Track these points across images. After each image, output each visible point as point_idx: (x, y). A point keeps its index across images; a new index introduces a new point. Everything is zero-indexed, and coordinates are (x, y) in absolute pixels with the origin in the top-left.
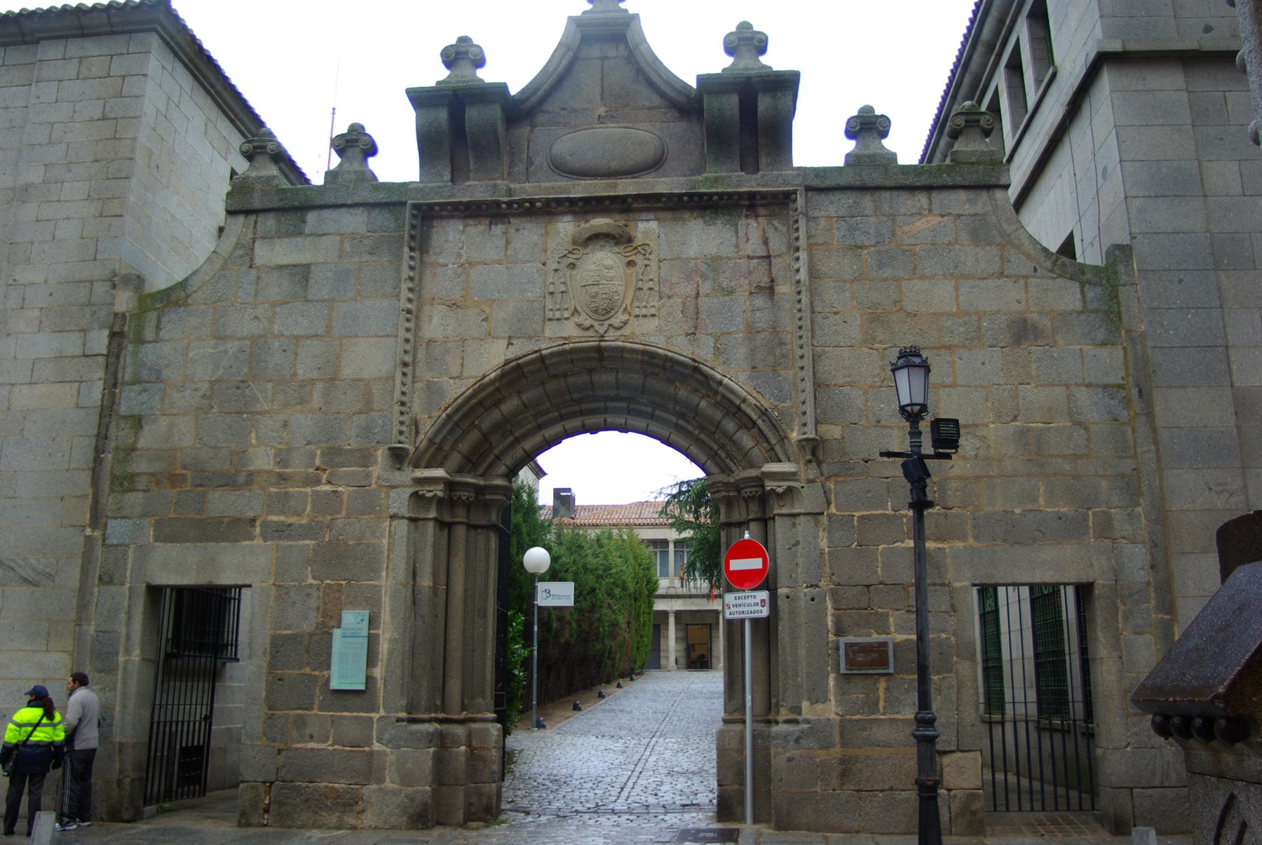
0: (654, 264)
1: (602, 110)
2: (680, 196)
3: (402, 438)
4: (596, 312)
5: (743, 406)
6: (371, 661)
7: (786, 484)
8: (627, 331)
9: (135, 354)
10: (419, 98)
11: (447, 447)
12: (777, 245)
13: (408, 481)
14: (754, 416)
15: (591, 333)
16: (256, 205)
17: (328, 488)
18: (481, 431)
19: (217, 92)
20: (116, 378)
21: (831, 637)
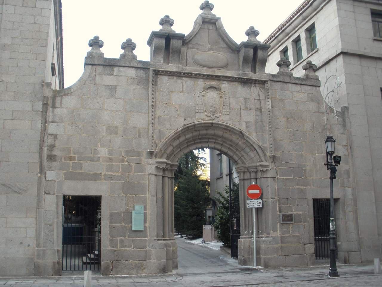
6: (145, 222)
7: (266, 168)
8: (221, 119)
9: (53, 112)
12: (262, 96)
15: (210, 118)
16: (96, 63)
17: (126, 163)
21: (278, 213)
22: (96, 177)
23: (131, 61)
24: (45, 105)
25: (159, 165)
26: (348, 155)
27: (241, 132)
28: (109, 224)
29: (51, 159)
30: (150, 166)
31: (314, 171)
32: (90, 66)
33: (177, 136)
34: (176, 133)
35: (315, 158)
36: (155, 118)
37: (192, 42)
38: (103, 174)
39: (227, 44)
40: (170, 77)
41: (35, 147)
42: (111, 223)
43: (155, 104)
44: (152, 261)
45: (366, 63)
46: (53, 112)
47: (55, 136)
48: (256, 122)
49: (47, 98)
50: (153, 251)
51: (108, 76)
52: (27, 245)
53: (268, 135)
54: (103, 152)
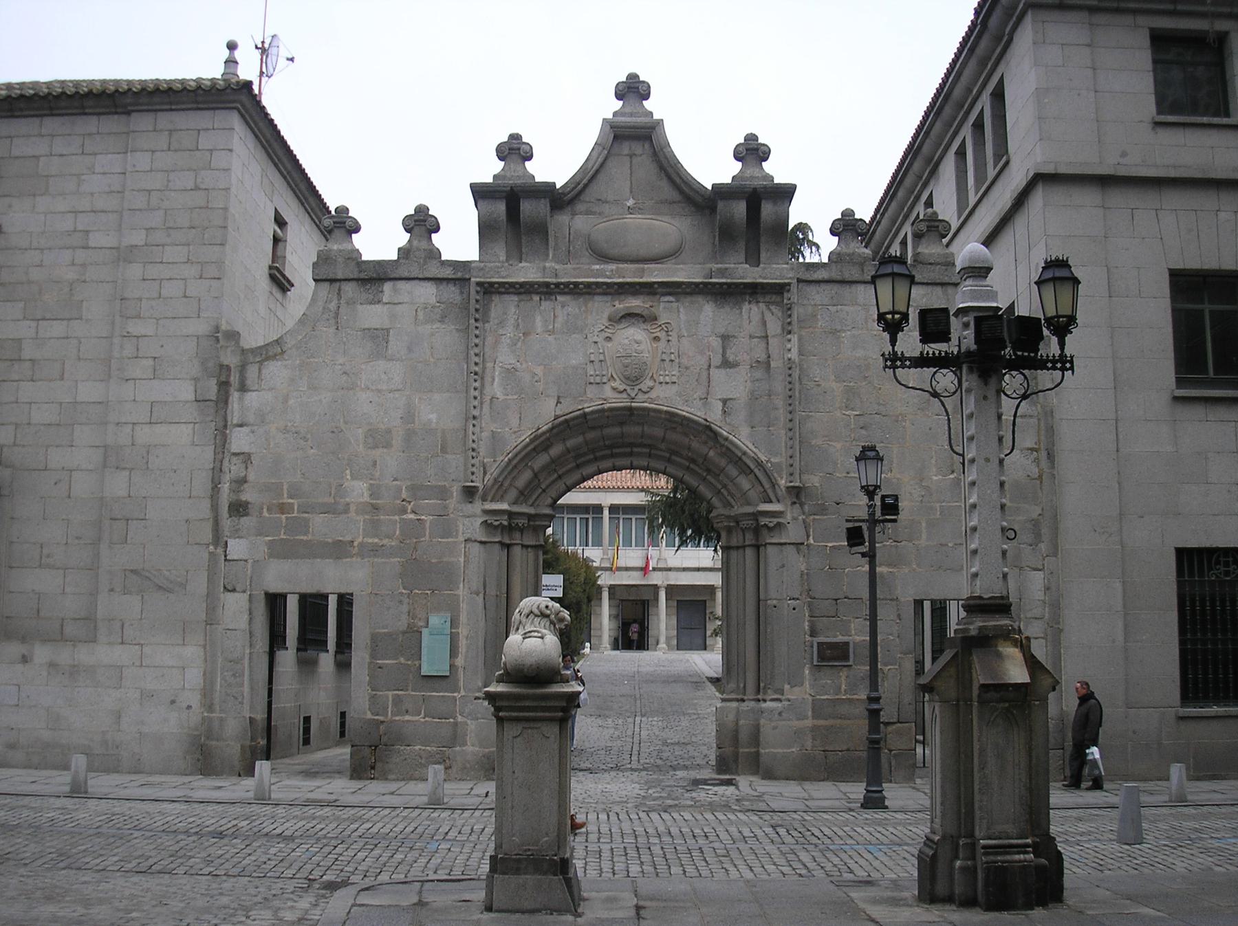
0: (674, 339)
1: (630, 203)
2: (697, 284)
3: (474, 478)
4: (628, 378)
5: (744, 458)
6: (453, 653)
7: (775, 520)
8: (653, 395)
9: (241, 399)
10: (480, 193)
11: (506, 484)
12: (774, 327)
13: (479, 512)
14: (752, 467)
15: (624, 395)
16: (340, 276)
17: (412, 516)
18: (533, 470)
19: (256, 124)
20: (226, 421)
21: (808, 638)
22: (339, 550)
23: (425, 263)
24: (224, 385)
25: (490, 519)
26: (1040, 477)
27: (709, 428)
28: (368, 660)
29: (238, 511)
30: (470, 522)
31: (924, 525)
32: (327, 284)
33: (541, 443)
34: (536, 438)
35: (927, 488)
36: (482, 403)
37: (585, 197)
38: (356, 544)
39: (681, 192)
40: (523, 297)
41: (202, 483)
42: (373, 656)
43: (484, 368)
44: (469, 748)
45: (1120, 199)
46: (241, 399)
47: (246, 458)
48: (753, 397)
49: (228, 368)
50: (472, 725)
51: (369, 307)
52: (185, 705)
53: (783, 432)
54: (358, 491)
